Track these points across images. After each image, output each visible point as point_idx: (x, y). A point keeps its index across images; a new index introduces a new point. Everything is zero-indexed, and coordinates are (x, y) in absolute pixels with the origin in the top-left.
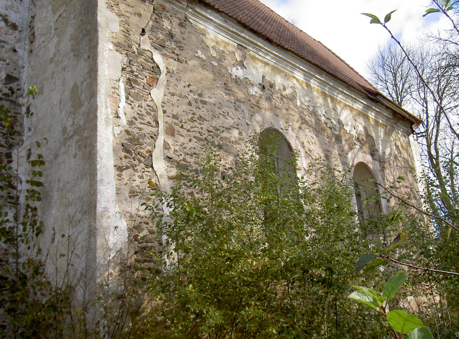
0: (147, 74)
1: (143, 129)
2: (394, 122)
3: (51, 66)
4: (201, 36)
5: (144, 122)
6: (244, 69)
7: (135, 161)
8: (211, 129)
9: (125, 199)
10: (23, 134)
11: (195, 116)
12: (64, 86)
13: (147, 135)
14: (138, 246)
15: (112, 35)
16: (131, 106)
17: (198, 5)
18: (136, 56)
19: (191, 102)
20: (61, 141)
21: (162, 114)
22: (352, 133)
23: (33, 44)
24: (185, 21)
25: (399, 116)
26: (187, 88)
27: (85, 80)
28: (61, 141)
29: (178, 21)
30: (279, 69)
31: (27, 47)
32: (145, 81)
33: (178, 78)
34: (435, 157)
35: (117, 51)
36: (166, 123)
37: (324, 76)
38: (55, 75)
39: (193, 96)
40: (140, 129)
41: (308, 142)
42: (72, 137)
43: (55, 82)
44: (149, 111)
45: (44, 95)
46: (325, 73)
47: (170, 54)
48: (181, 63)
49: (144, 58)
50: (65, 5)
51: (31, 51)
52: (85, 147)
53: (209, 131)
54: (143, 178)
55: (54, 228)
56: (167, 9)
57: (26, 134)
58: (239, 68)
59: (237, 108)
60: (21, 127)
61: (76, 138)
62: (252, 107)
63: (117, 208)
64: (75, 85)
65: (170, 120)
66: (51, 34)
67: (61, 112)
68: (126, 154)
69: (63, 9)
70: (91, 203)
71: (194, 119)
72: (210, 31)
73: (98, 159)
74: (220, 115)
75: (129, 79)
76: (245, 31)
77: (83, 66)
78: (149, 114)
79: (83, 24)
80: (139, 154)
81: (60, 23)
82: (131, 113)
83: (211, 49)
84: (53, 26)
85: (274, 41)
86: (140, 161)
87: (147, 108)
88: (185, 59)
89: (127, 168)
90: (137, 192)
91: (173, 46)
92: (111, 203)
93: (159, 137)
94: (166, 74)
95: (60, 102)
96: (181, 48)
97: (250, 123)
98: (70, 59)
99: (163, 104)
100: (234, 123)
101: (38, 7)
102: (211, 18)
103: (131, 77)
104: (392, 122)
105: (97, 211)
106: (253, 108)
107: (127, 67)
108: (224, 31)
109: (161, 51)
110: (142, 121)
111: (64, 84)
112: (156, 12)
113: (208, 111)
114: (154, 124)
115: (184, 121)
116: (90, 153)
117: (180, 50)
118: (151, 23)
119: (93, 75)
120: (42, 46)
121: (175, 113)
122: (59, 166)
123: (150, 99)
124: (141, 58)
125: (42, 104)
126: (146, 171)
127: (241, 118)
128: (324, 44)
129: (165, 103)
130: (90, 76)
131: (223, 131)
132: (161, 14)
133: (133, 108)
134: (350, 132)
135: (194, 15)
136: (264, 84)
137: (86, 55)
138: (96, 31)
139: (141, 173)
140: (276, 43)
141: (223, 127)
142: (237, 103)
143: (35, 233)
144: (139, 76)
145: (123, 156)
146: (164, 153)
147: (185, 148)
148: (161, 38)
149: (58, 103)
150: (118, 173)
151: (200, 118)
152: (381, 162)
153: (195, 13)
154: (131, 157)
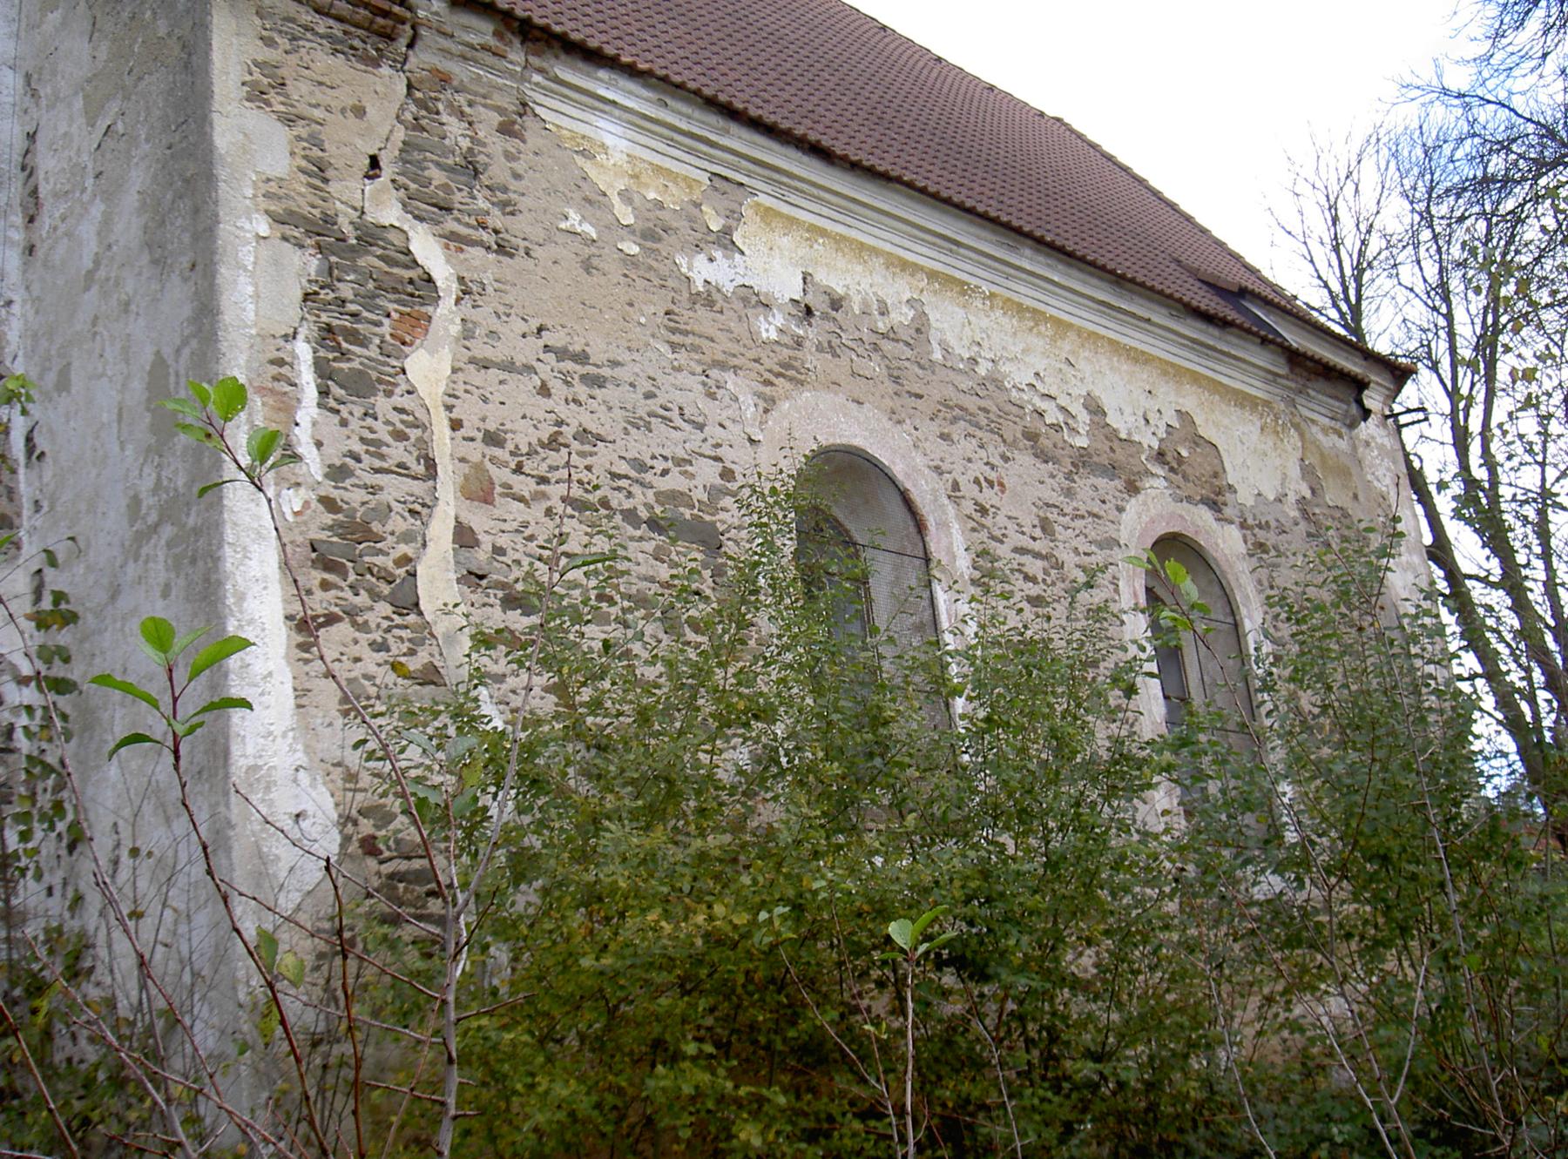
0: (391, 307)
1: (381, 489)
2: (1293, 385)
3: (86, 296)
4: (579, 160)
5: (385, 465)
6: (737, 256)
7: (357, 595)
8: (623, 468)
9: (327, 721)
10: (16, 522)
11: (564, 429)
12: (127, 362)
13: (396, 507)
14: (379, 874)
15: (264, 188)
16: (336, 419)
17: (563, 57)
18: (352, 249)
19: (550, 385)
20: (127, 543)
21: (448, 432)
22: (1136, 438)
23: (36, 224)
24: (521, 116)
25: (1309, 364)
26: (531, 339)
27: (185, 342)
28: (127, 543)
29: (496, 119)
30: (862, 244)
31: (17, 236)
32: (386, 329)
33: (501, 309)
34: (1487, 485)
35: (285, 238)
36: (462, 460)
37: (1028, 252)
38: (99, 329)
39: (554, 363)
40: (374, 490)
41: (977, 481)
42: (155, 528)
43: (103, 350)
44: (400, 426)
45: (73, 391)
46: (1029, 242)
47: (470, 231)
48: (511, 256)
49: (380, 252)
50: (119, 96)
51: (31, 250)
52: (193, 561)
53: (615, 476)
54: (388, 650)
55: (115, 824)
56: (455, 83)
57: (27, 519)
58: (718, 254)
59: (714, 389)
60: (11, 500)
61: (168, 531)
62: (768, 383)
63: (300, 755)
64: (159, 362)
65: (476, 451)
66: (84, 190)
67: (122, 449)
68: (327, 576)
69: (114, 107)
70: (214, 742)
71: (561, 440)
72: (609, 141)
73: (230, 601)
74: (653, 420)
75: (329, 329)
76: (734, 128)
77: (178, 298)
78: (400, 436)
79: (172, 156)
80: (370, 570)
81: (108, 156)
82: (342, 442)
83: (616, 200)
84: (90, 166)
85: (839, 152)
86: (375, 596)
87: (395, 418)
88: (523, 244)
89: (331, 619)
90: (368, 698)
91: (482, 204)
92: (279, 740)
93: (441, 505)
94: (458, 301)
95: (120, 415)
96: (508, 209)
97: (760, 437)
98: (140, 274)
99: (451, 401)
100: (705, 440)
101: (44, 102)
102: (610, 95)
103: (335, 322)
104: (1290, 388)
105: (233, 769)
106: (772, 384)
107: (322, 288)
108: (661, 136)
109: (438, 223)
110: (378, 463)
111: (126, 355)
112: (418, 95)
113: (610, 409)
114: (420, 469)
115: (524, 450)
116: (207, 580)
117: (504, 214)
118: (400, 134)
119: (207, 327)
120: (59, 232)
121: (492, 426)
122: (123, 625)
123: (404, 387)
124: (368, 253)
125: (68, 421)
126: (397, 626)
127: (727, 423)
128: (1075, 126)
129: (457, 397)
130: (200, 330)
131: (665, 473)
132: (437, 99)
133: (344, 423)
134: (1129, 434)
135: (552, 91)
136: (809, 300)
137: (185, 261)
138: (210, 178)
139: (380, 633)
140: (844, 158)
141: (666, 458)
142: (714, 373)
143: (65, 842)
144: (365, 314)
145: (317, 582)
146: (457, 563)
147: (531, 538)
148: (435, 183)
149: (115, 417)
150: (300, 639)
151: (583, 434)
152: (1250, 528)
153: (554, 86)
154: (343, 584)
